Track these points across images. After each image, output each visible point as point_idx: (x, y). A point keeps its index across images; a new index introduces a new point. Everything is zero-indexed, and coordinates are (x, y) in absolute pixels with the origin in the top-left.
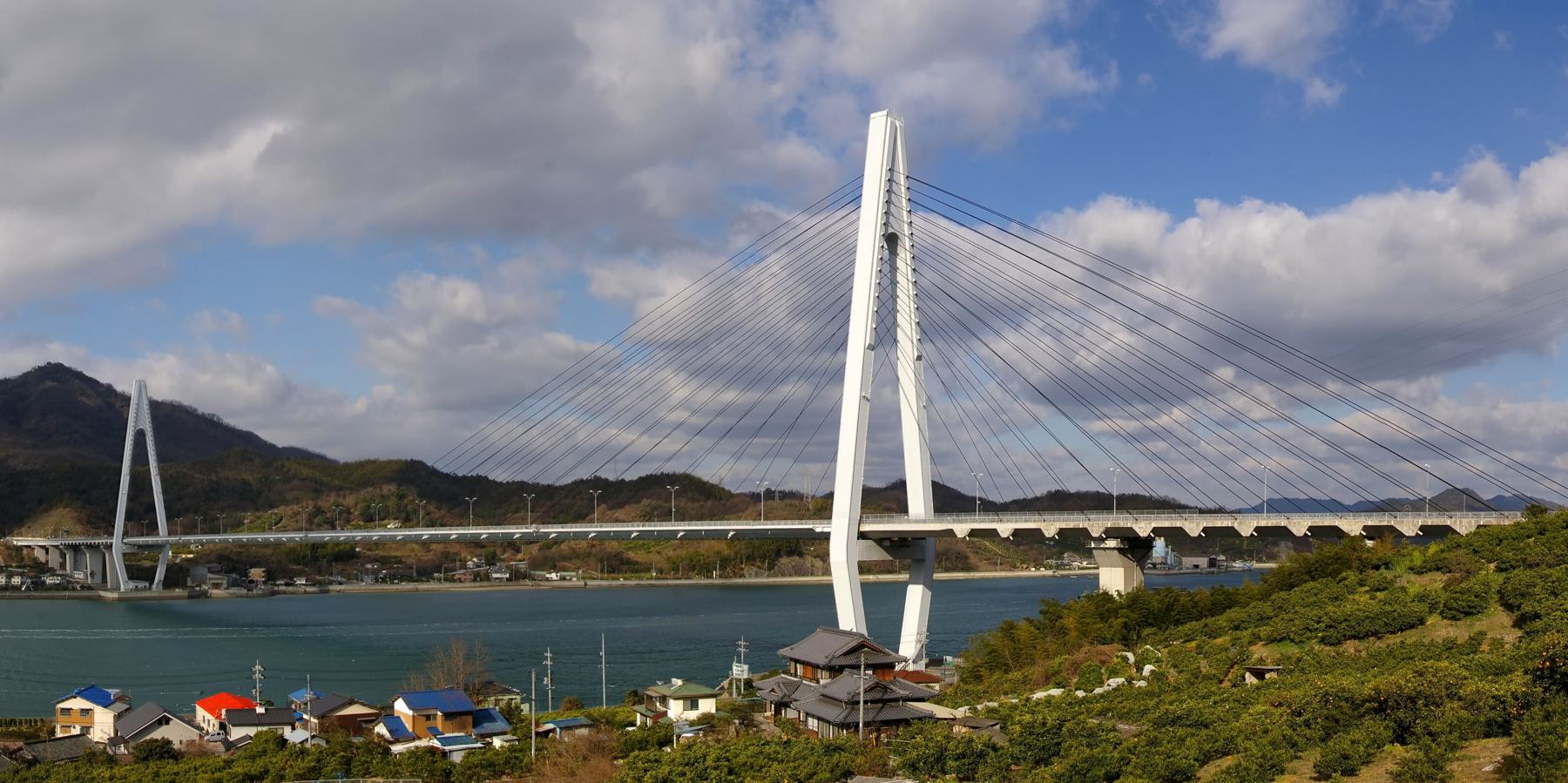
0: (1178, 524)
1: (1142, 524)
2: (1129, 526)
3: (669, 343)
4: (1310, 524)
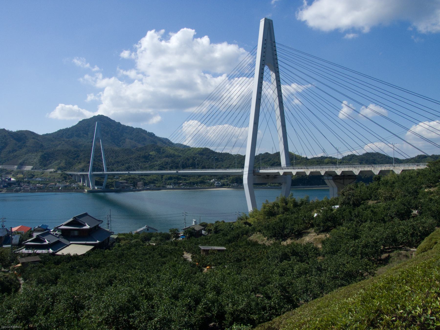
0: (351, 169)
1: (338, 170)
2: (334, 170)
3: (237, 107)
4: (403, 169)
